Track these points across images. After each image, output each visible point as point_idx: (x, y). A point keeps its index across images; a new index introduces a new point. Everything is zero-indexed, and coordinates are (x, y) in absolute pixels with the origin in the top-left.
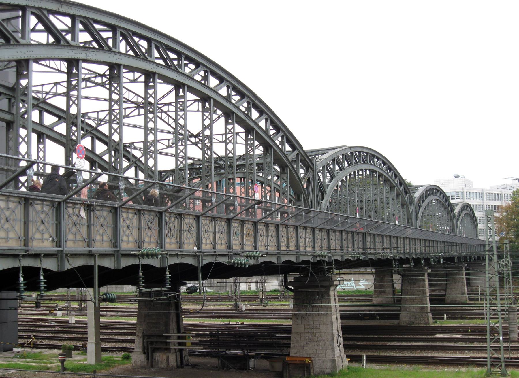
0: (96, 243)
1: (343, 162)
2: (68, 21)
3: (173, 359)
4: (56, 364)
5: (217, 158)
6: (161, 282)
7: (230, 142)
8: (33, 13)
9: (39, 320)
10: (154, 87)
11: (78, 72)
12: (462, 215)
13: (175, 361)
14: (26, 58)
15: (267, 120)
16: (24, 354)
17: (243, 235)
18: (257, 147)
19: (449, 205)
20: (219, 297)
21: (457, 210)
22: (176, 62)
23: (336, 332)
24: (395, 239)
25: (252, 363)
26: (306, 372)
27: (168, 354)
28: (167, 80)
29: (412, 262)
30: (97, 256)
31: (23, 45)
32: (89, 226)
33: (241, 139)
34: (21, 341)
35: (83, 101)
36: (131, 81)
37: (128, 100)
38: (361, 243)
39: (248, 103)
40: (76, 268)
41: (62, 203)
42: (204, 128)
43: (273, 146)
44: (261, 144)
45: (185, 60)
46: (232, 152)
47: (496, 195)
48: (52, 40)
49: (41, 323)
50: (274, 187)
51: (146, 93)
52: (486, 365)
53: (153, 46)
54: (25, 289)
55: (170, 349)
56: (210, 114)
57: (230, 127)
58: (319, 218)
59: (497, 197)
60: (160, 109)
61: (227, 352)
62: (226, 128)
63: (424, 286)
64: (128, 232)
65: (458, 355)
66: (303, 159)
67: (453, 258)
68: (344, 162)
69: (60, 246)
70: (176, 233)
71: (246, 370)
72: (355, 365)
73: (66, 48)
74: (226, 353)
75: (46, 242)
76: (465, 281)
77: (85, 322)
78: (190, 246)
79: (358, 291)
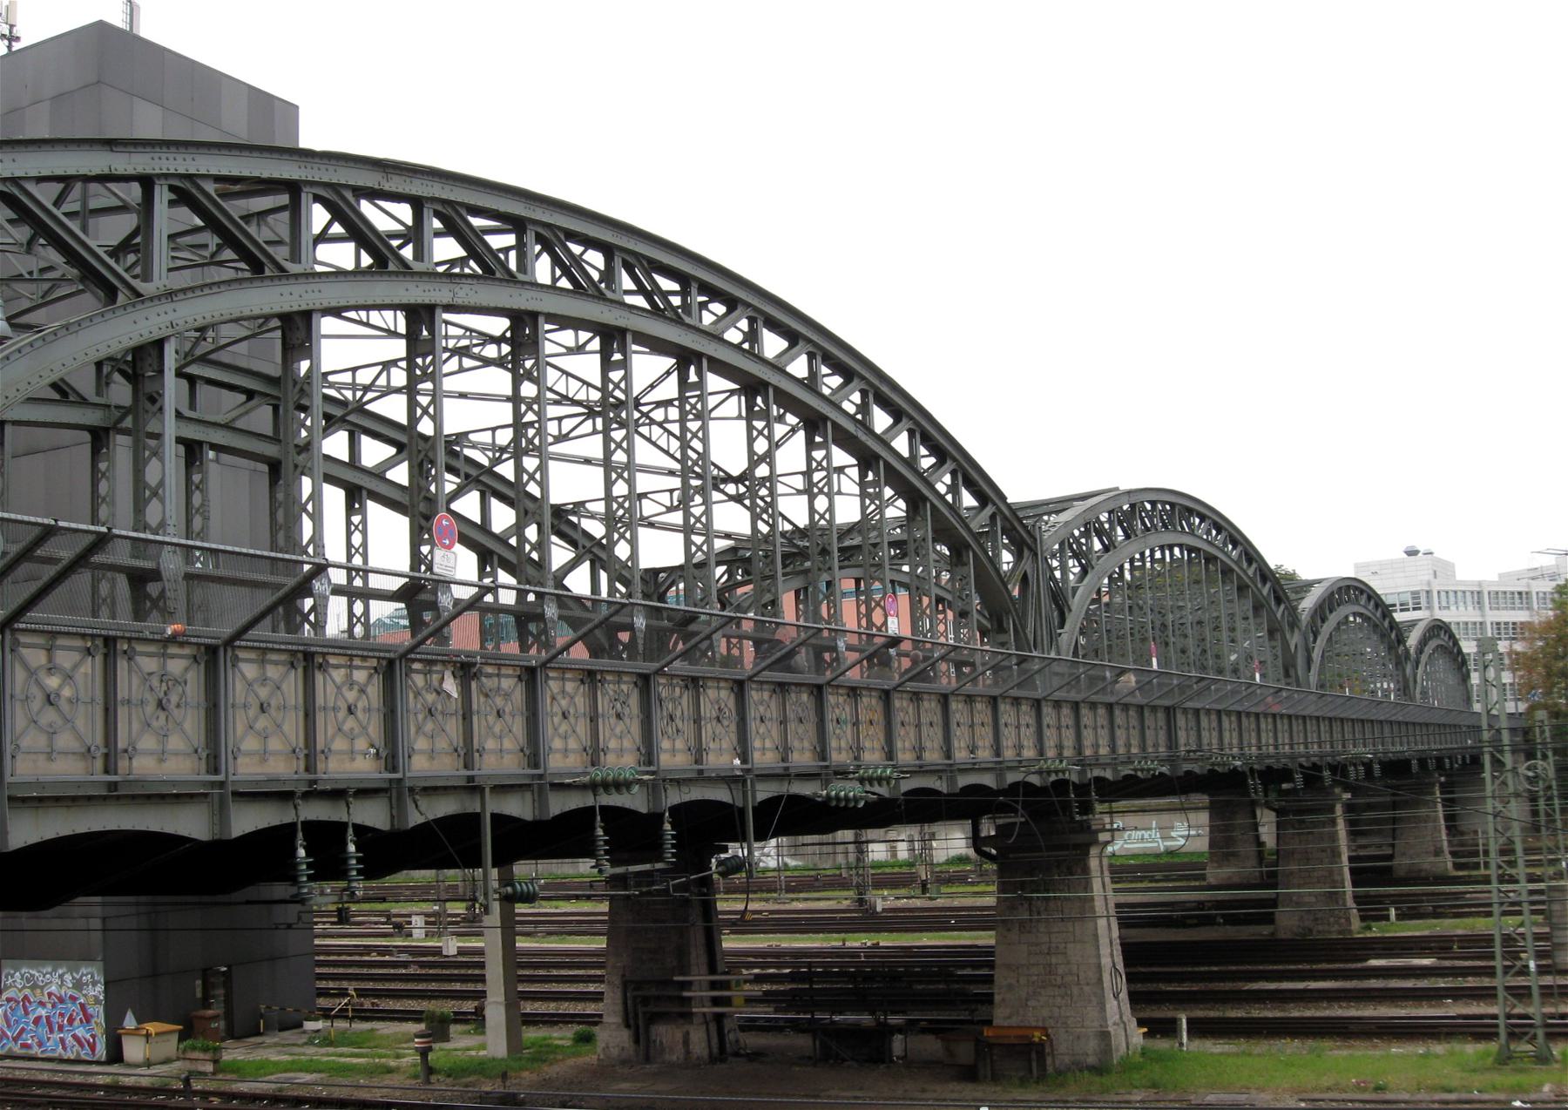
0: (485, 757)
1: (1112, 528)
2: (404, 212)
3: (699, 1042)
4: (411, 1059)
5: (793, 532)
6: (652, 849)
7: (821, 491)
8: (318, 199)
9: (368, 950)
10: (625, 364)
11: (434, 336)
12: (1428, 650)
13: (704, 1044)
14: (304, 307)
15: (911, 433)
16: (330, 1033)
17: (856, 724)
18: (890, 502)
19: (1392, 628)
20: (817, 880)
21: (1412, 640)
22: (676, 301)
23: (1109, 960)
24: (1252, 719)
25: (898, 1044)
26: (1034, 1064)
27: (687, 1027)
28: (658, 346)
29: (1298, 777)
30: (487, 790)
31: (296, 276)
32: (467, 716)
33: (849, 484)
34: (323, 1002)
35: (449, 405)
36: (571, 351)
37: (566, 397)
38: (1162, 735)
39: (864, 394)
40: (438, 821)
41: (398, 663)
42: (754, 460)
43: (931, 497)
44: (899, 493)
45: (700, 294)
46: (827, 516)
47: (1516, 596)
48: (366, 260)
49: (374, 957)
51: (605, 379)
52: (1497, 1035)
53: (618, 262)
54: (311, 878)
55: (691, 1014)
56: (768, 426)
57: (818, 455)
58: (1057, 674)
59: (1517, 601)
60: (646, 415)
61: (837, 1018)
62: (809, 459)
63: (1333, 837)
64: (564, 728)
65: (1426, 1011)
66: (1008, 525)
67: (1407, 762)
68: (1115, 530)
69: (394, 769)
70: (688, 728)
71: (883, 1062)
72: (1162, 1044)
73: (401, 278)
74: (833, 1023)
75: (359, 758)
76: (1442, 822)
77: (480, 952)
78: (722, 758)
79: (1170, 853)
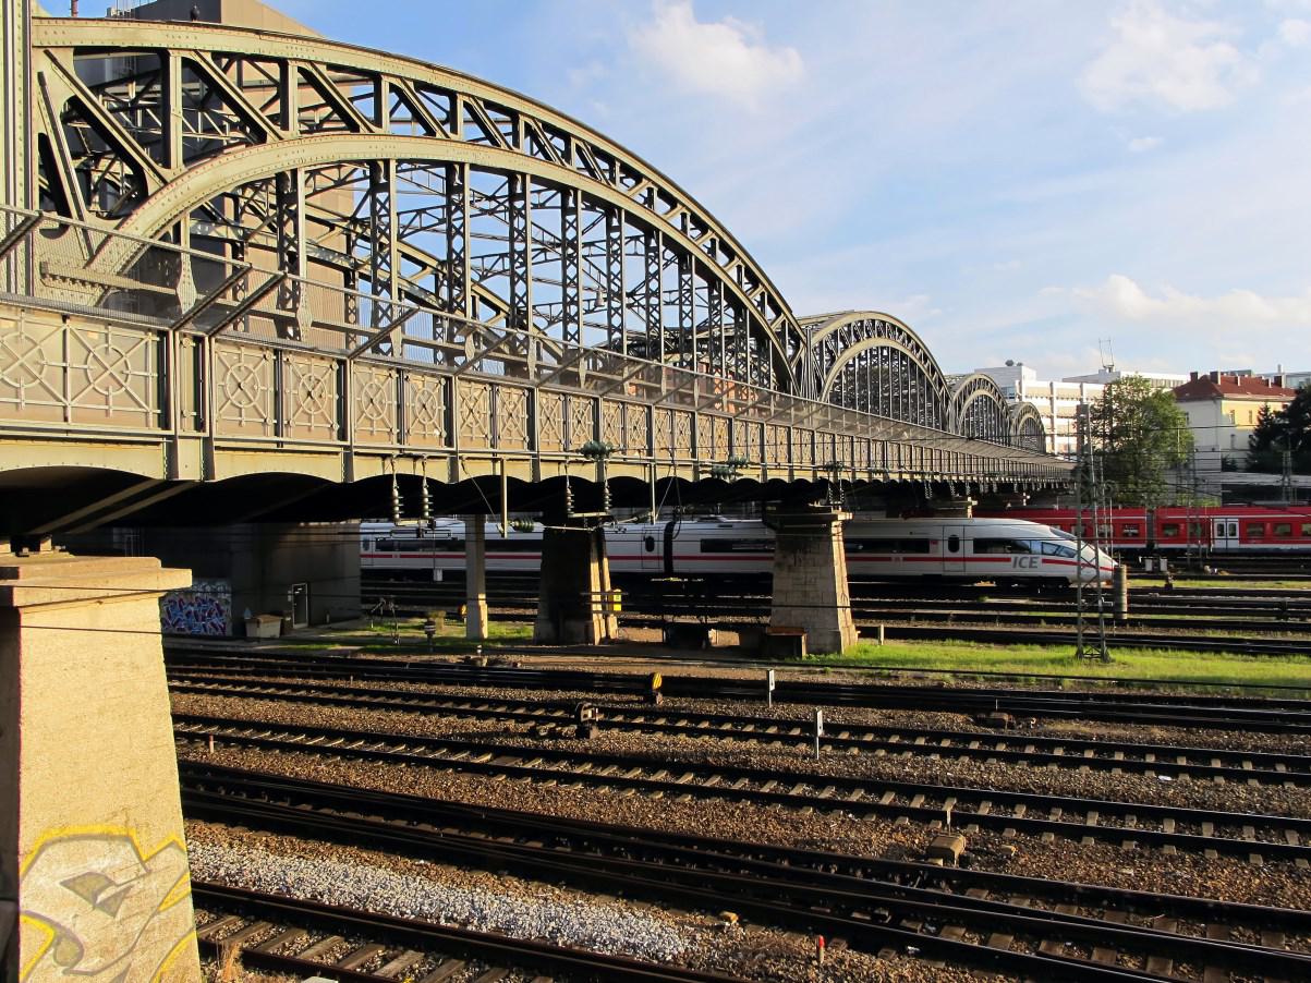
40: (478, 479)
50: (400, 290)
62: (681, 279)
